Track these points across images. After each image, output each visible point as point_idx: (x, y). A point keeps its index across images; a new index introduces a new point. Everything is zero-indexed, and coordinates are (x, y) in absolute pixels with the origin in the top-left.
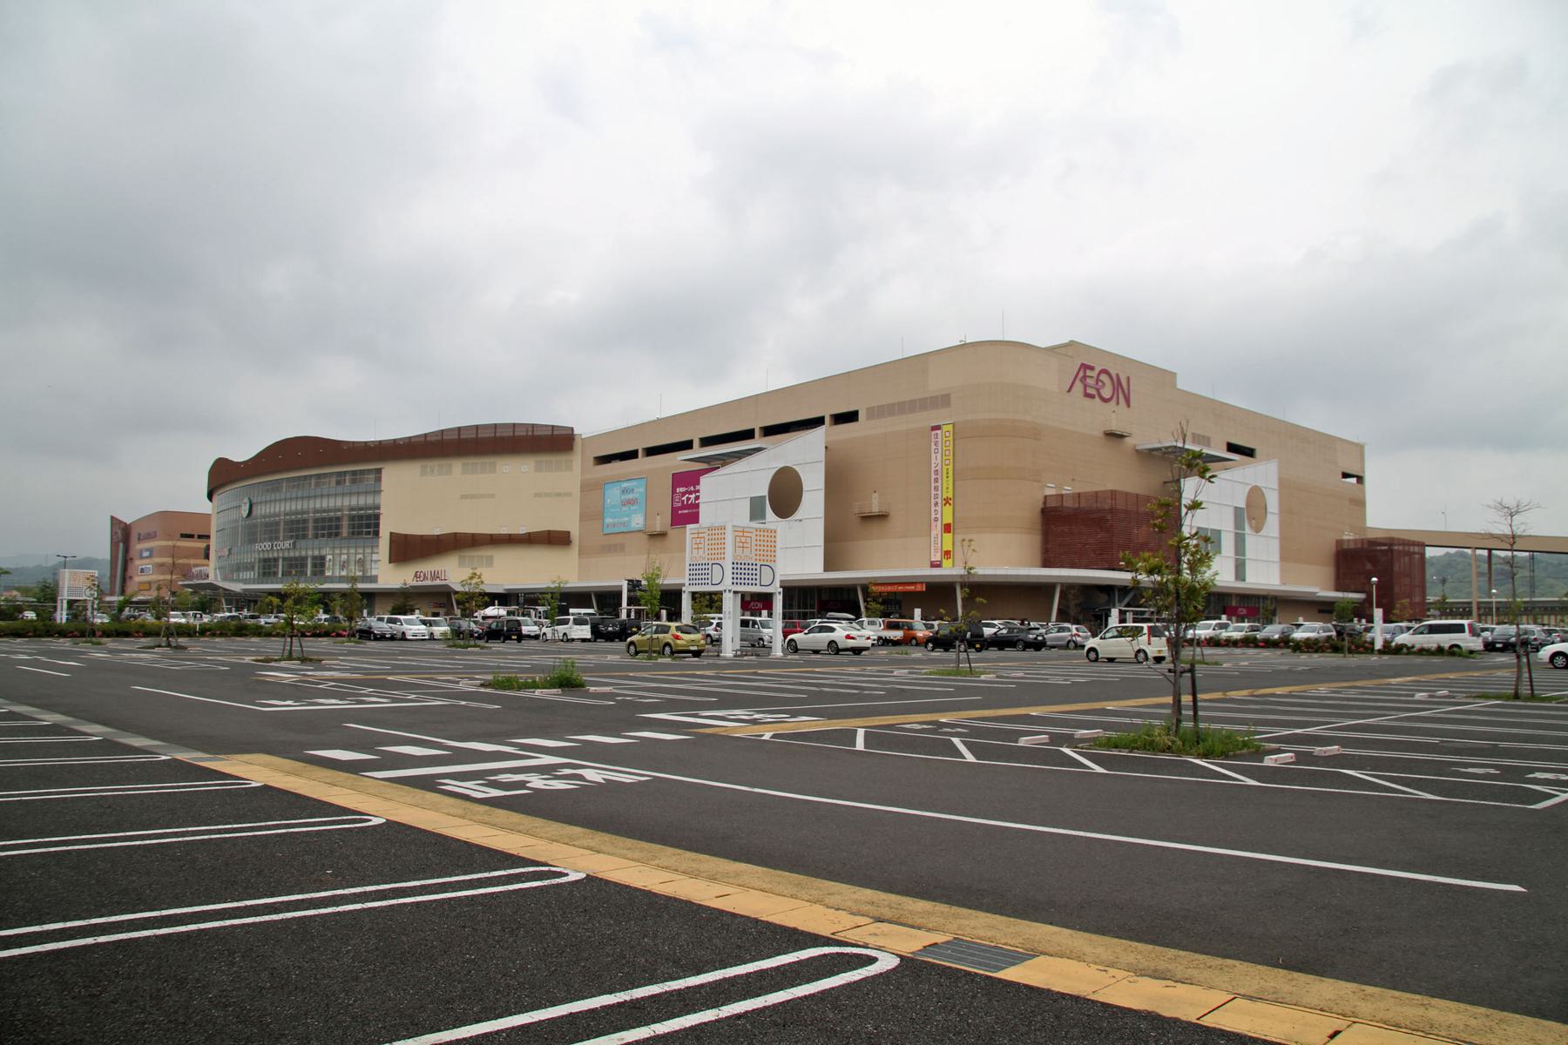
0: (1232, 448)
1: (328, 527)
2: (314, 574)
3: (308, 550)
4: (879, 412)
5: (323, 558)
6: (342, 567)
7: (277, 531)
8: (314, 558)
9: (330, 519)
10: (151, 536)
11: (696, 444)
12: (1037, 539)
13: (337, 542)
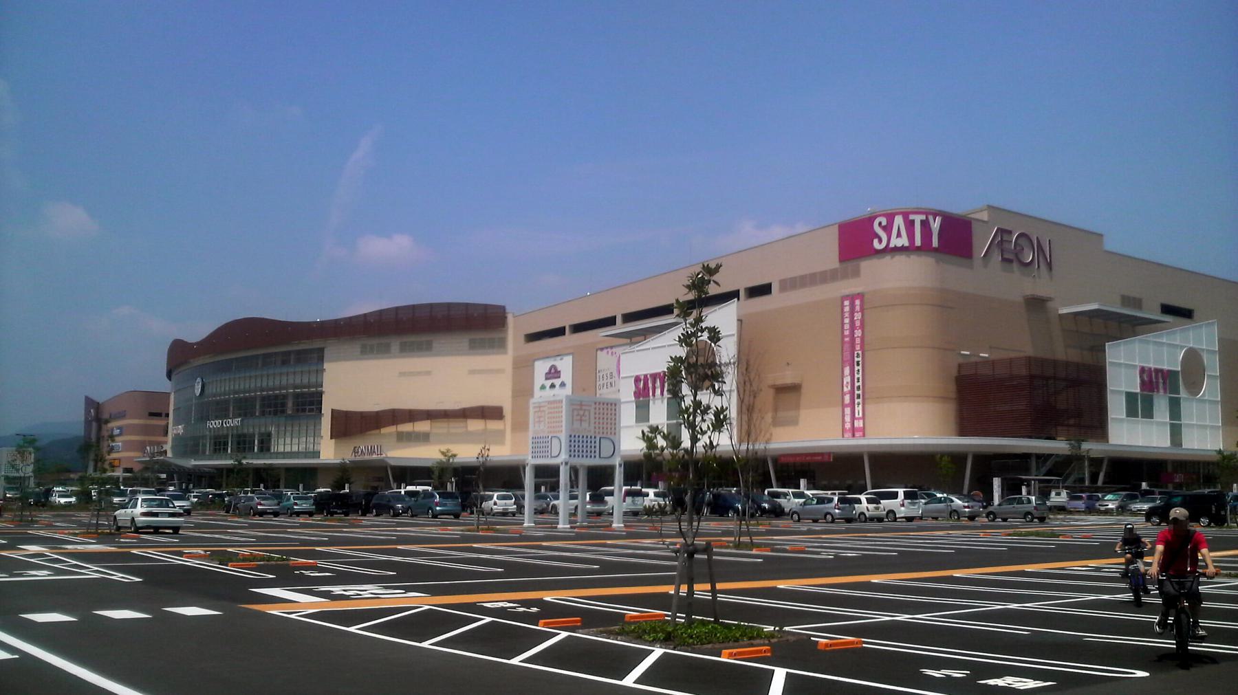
0: (1167, 309)
1: (274, 406)
2: (261, 449)
3: (255, 427)
4: (790, 284)
5: (269, 435)
6: (288, 448)
7: (227, 410)
8: (261, 435)
9: (276, 397)
10: (122, 416)
11: (619, 320)
12: (950, 409)
13: (282, 420)
